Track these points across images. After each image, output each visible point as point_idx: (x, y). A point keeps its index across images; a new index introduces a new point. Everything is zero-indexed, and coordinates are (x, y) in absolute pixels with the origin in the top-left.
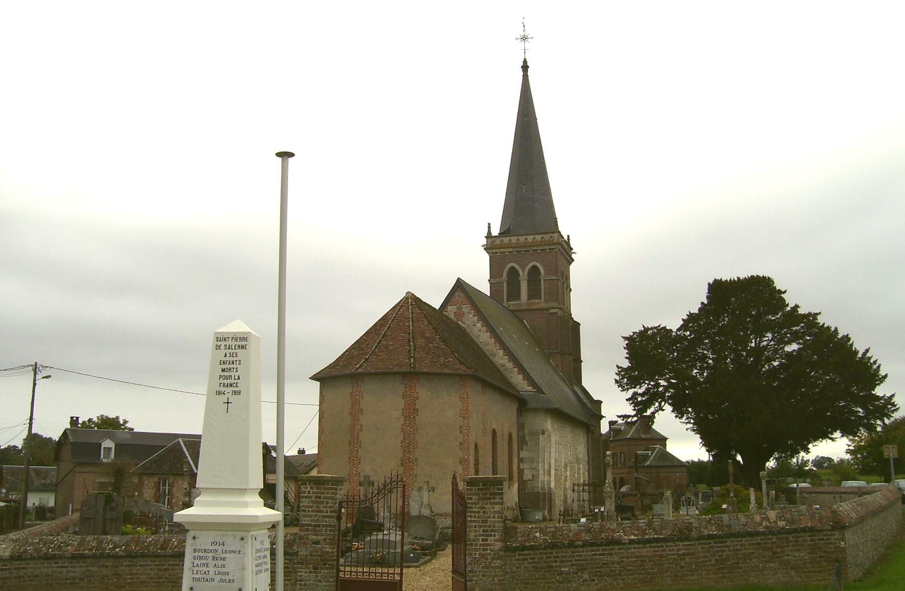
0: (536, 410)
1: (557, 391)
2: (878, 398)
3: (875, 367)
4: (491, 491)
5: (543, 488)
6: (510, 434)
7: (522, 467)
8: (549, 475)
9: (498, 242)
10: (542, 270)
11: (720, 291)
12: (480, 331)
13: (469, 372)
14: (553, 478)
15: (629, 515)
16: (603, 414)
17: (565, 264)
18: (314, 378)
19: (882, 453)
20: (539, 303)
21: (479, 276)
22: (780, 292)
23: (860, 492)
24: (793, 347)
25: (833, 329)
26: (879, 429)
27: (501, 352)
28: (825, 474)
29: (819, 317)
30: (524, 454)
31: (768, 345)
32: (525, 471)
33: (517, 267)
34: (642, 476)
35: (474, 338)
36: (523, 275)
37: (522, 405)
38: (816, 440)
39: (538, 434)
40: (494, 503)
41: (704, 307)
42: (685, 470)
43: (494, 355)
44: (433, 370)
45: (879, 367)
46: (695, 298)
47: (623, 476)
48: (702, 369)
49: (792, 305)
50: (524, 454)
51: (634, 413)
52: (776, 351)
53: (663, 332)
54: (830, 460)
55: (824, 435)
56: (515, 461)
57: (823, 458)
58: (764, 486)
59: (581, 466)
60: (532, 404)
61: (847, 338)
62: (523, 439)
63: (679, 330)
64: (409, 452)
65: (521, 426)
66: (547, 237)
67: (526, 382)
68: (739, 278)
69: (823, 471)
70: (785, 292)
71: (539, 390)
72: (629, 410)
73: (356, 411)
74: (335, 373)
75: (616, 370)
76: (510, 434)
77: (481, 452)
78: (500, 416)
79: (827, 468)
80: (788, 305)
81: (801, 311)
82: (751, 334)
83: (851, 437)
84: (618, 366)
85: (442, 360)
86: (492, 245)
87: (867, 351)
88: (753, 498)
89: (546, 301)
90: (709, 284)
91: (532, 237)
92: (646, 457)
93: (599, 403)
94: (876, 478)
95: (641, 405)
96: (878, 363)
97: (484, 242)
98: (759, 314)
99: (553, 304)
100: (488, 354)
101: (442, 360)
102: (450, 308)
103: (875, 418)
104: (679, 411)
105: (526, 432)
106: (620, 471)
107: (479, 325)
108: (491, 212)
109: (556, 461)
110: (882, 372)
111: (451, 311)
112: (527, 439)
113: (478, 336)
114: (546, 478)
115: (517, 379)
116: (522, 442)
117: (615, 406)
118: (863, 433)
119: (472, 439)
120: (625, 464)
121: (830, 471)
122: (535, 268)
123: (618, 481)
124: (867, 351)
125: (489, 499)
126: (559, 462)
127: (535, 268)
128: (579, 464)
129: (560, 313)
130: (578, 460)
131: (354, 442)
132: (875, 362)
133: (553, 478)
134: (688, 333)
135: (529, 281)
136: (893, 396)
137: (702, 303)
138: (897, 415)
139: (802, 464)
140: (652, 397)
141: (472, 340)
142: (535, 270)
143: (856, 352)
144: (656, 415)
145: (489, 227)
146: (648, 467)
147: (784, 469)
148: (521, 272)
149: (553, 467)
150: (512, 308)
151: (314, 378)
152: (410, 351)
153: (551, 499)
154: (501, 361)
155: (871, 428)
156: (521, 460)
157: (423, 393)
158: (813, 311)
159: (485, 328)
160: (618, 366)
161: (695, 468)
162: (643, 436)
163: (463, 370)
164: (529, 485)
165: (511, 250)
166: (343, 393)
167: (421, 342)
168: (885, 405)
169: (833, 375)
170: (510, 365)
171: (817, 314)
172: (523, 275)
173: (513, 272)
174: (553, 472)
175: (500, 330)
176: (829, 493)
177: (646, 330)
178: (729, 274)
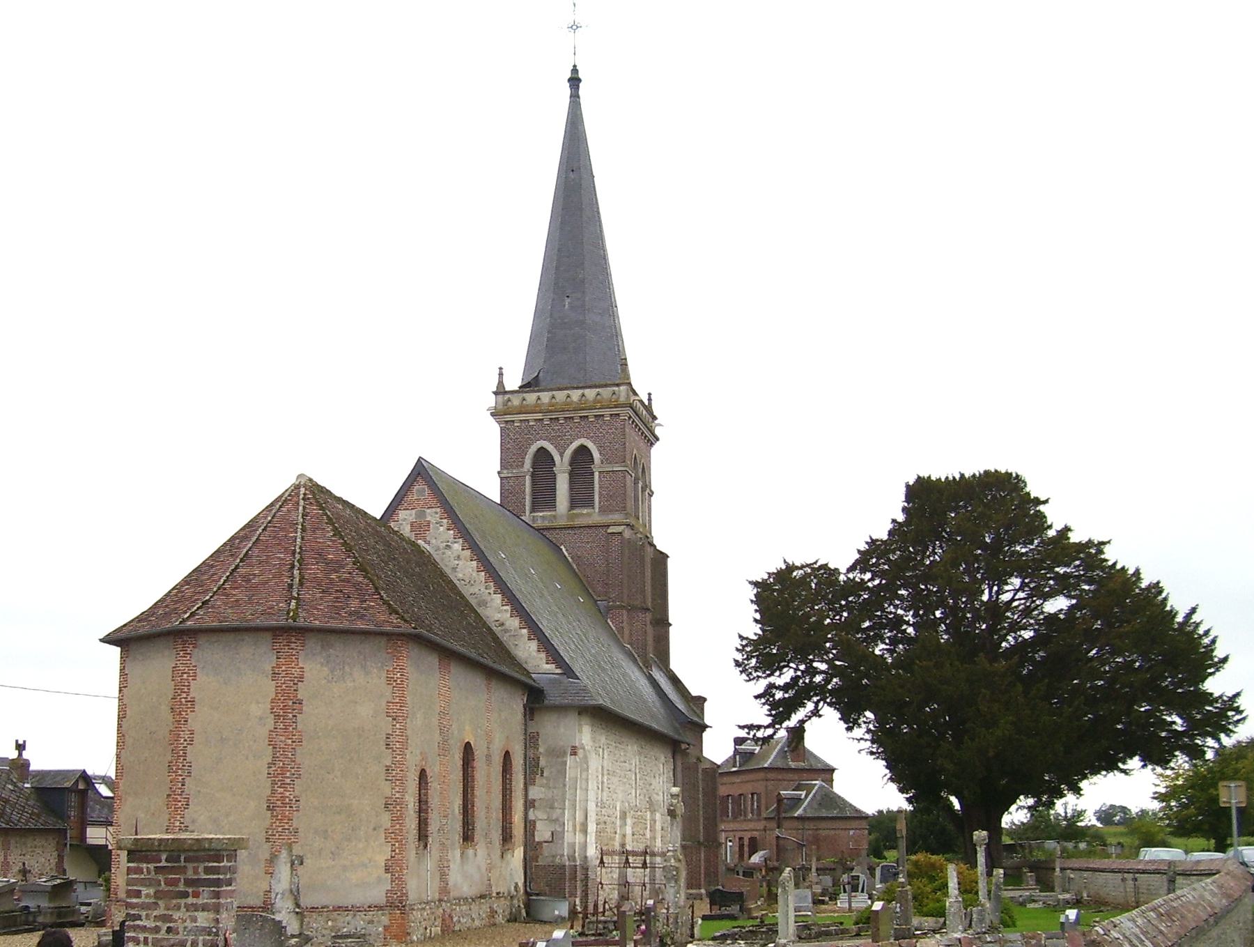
0: (562, 709)
1: (612, 674)
2: (1207, 698)
3: (1206, 641)
4: (190, 874)
5: (572, 857)
6: (507, 755)
7: (531, 816)
8: (585, 831)
9: (516, 401)
10: (596, 455)
11: (926, 497)
12: (458, 558)
13: (406, 628)
14: (591, 838)
15: (734, 909)
16: (707, 721)
17: (642, 444)
18: (109, 640)
19: (1215, 800)
20: (589, 515)
21: (478, 465)
22: (1037, 502)
23: (1172, 875)
24: (1057, 605)
25: (1131, 572)
26: (1210, 755)
27: (498, 598)
28: (1115, 835)
29: (1106, 549)
30: (535, 792)
31: (1013, 600)
32: (539, 825)
33: (550, 448)
34: (789, 834)
35: (448, 571)
36: (562, 464)
37: (535, 699)
38: (1096, 772)
39: (565, 753)
40: (196, 908)
41: (897, 530)
42: (864, 824)
43: (483, 603)
44: (333, 624)
45: (1214, 641)
46: (882, 513)
47: (756, 834)
48: (894, 642)
49: (1058, 526)
50: (535, 792)
51: (769, 720)
52: (1027, 612)
53: (826, 574)
54: (1124, 810)
55: (1110, 764)
56: (518, 805)
57: (1112, 807)
58: (981, 858)
59: (658, 816)
60: (553, 697)
61: (1156, 588)
62: (533, 764)
63: (851, 569)
64: (283, 785)
65: (531, 741)
66: (606, 393)
67: (543, 655)
68: (962, 476)
69: (1113, 829)
70: (1046, 502)
71: (568, 672)
72: (760, 715)
73: (181, 705)
74: (145, 629)
75: (738, 643)
76: (507, 755)
77: (434, 786)
78: (490, 719)
79: (1119, 823)
80: (1050, 527)
81: (1074, 538)
82: (983, 579)
83: (1159, 770)
84: (740, 636)
85: (354, 604)
86: (507, 410)
87: (1193, 610)
88: (953, 884)
89: (603, 510)
90: (908, 486)
91: (580, 392)
92: (797, 801)
93: (701, 700)
94: (1202, 842)
95: (781, 711)
96: (1212, 634)
97: (491, 401)
98: (998, 541)
99: (617, 517)
100: (473, 602)
101: (354, 604)
102: (403, 515)
103: (1204, 735)
104: (850, 719)
105: (541, 750)
106: (751, 825)
107: (457, 547)
108: (503, 342)
109: (601, 805)
110: (1219, 653)
111: (404, 522)
112: (542, 762)
113: (454, 569)
114: (579, 838)
115: (528, 651)
116: (533, 770)
117: (732, 710)
118: (1181, 761)
119: (412, 762)
120: (759, 814)
121: (1121, 829)
122: (583, 450)
123: (746, 842)
124: (1193, 610)
125: (185, 895)
126: (611, 804)
127: (583, 450)
128: (653, 812)
129: (627, 534)
130: (652, 806)
131: (178, 765)
132: (1207, 633)
133: (591, 838)
134: (868, 576)
135: (572, 475)
136: (1237, 695)
137: (894, 521)
138: (1243, 733)
139: (1073, 816)
140: (798, 695)
141: (442, 575)
142: (583, 451)
143: (1172, 614)
144: (806, 725)
145: (501, 374)
146: (799, 818)
147: (1040, 827)
148: (557, 458)
149: (592, 817)
150: (539, 524)
151: (109, 640)
152: (291, 586)
153: (587, 877)
154: (498, 616)
155: (1195, 753)
156: (529, 804)
157: (313, 667)
158: (1097, 538)
159: (468, 553)
160: (740, 636)
161: (883, 824)
162: (793, 765)
163: (393, 623)
164: (546, 850)
165: (539, 416)
166: (159, 667)
167: (314, 569)
168: (1222, 714)
169: (1131, 661)
170: (514, 623)
171: (1104, 543)
172: (562, 464)
173: (543, 458)
174: (592, 827)
175: (498, 558)
176: (1113, 871)
177: (790, 568)
178: (943, 468)
